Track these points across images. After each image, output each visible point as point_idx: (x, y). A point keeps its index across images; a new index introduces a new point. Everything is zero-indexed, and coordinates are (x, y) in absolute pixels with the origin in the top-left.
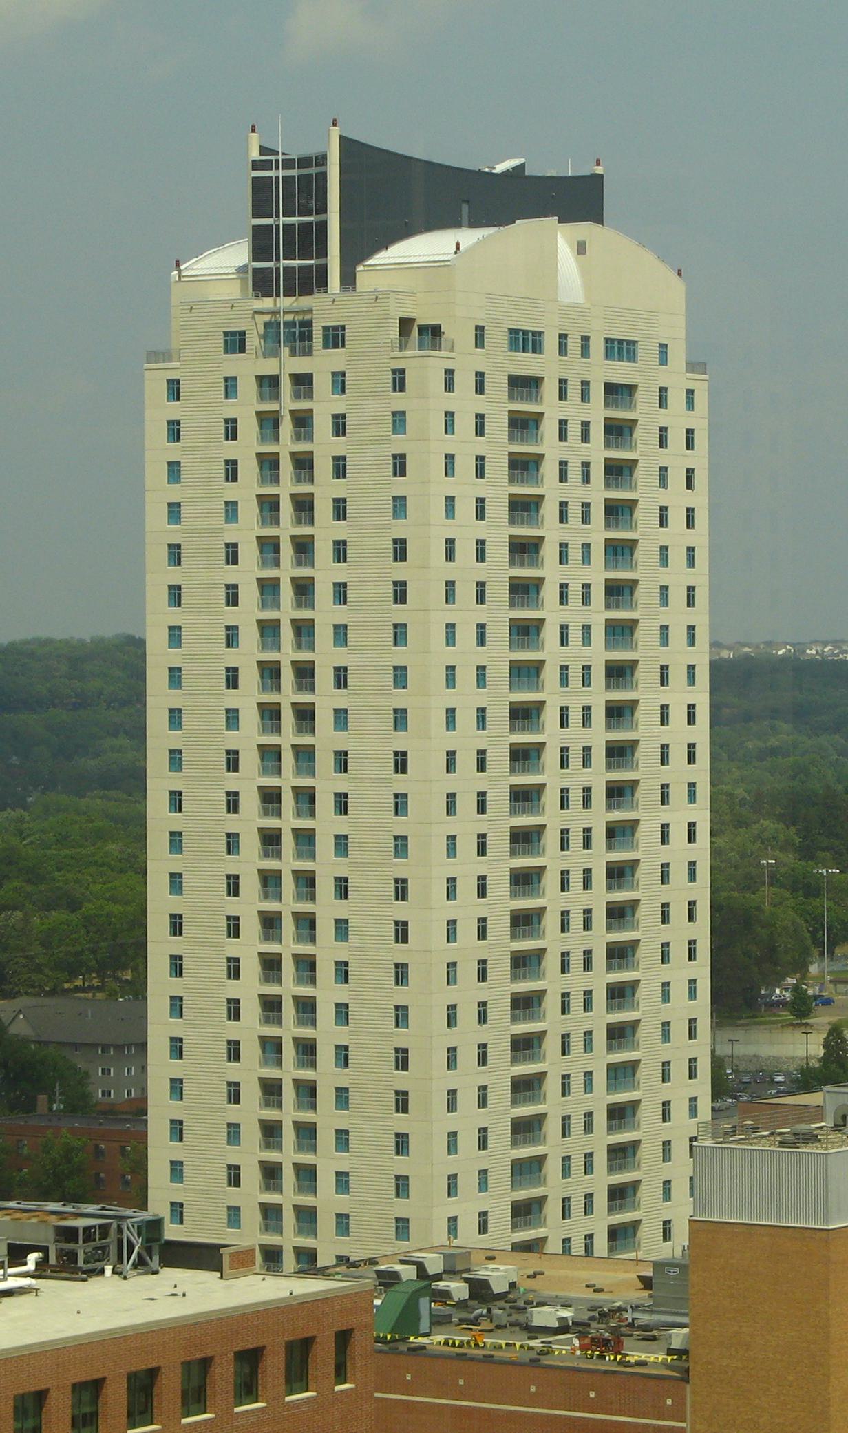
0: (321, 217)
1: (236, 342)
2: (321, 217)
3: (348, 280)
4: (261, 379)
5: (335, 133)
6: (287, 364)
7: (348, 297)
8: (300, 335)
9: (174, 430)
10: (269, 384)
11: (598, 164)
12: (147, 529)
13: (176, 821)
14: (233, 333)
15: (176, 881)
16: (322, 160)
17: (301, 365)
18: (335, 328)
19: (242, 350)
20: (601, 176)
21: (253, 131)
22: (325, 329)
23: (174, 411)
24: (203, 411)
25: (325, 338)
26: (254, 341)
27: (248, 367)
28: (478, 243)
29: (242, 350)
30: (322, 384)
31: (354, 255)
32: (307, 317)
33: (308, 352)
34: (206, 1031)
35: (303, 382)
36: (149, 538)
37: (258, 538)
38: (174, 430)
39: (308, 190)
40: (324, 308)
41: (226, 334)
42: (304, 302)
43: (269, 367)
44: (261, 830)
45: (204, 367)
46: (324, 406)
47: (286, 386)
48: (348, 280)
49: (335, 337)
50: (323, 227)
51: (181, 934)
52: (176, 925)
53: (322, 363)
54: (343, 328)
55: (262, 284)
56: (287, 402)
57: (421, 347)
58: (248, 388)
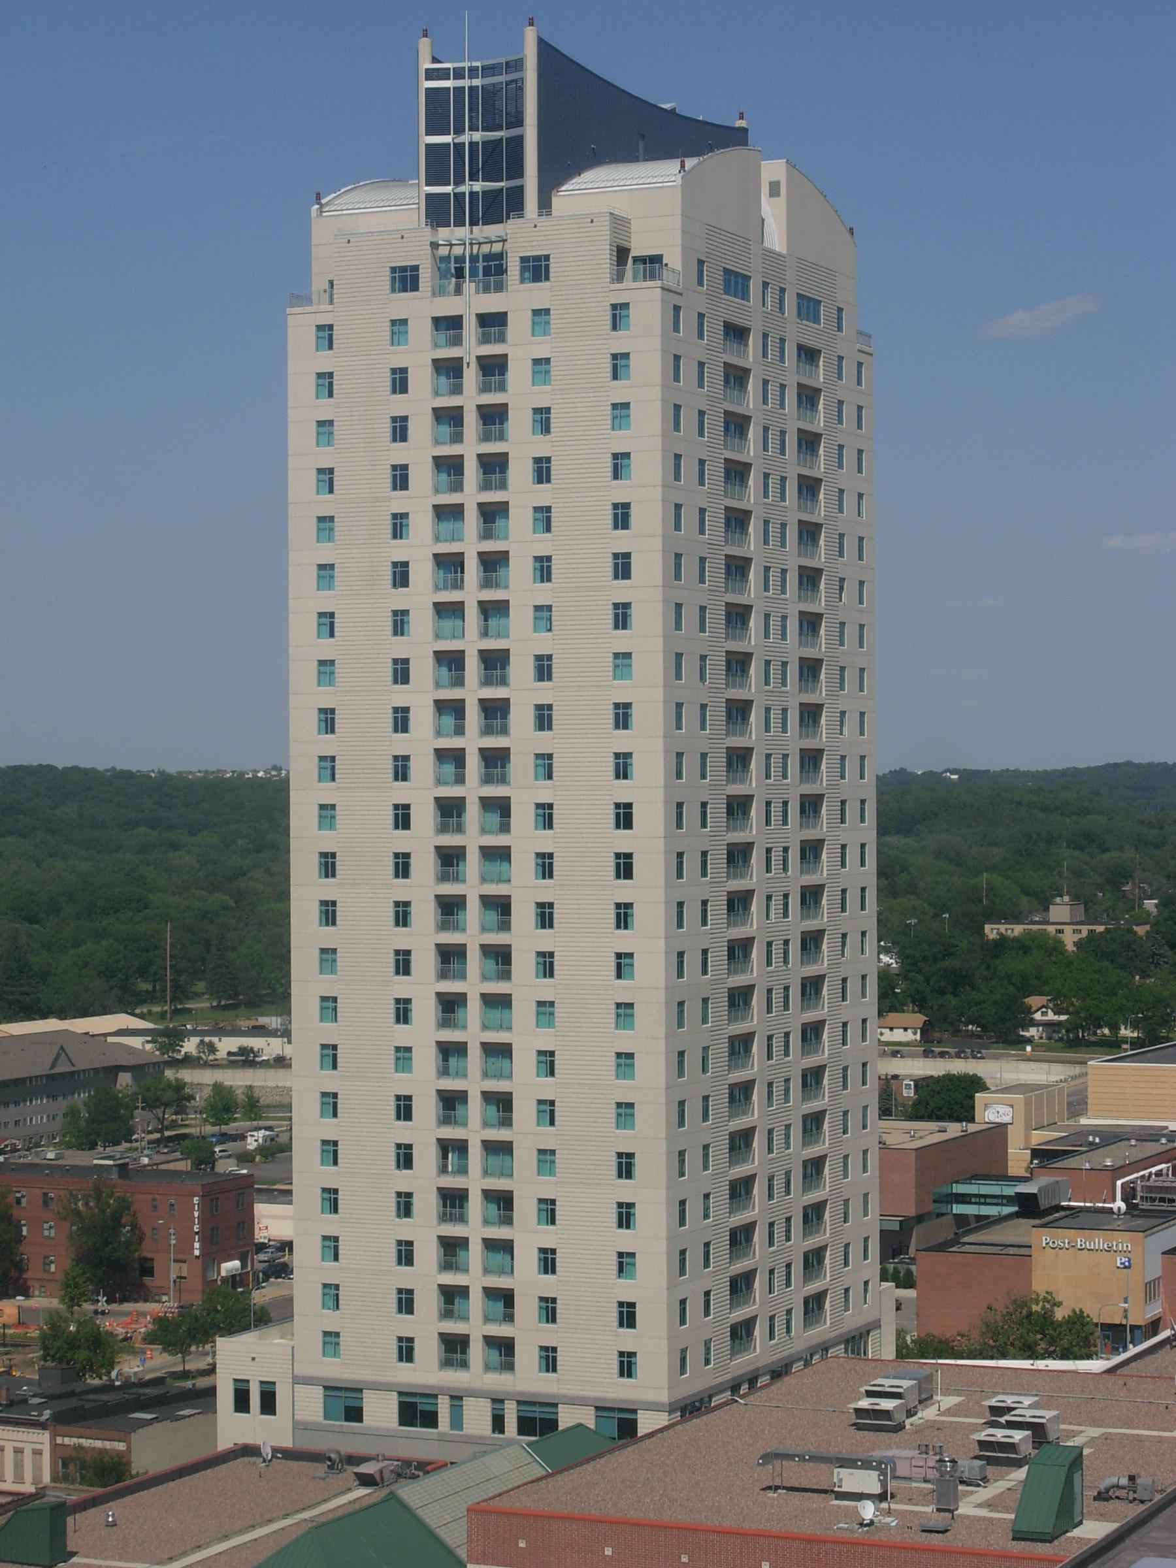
0: (514, 132)
1: (406, 279)
2: (514, 132)
3: (545, 204)
4: (438, 322)
5: (530, 37)
6: (472, 302)
7: (544, 222)
8: (492, 269)
9: (328, 622)
10: (449, 325)
11: (741, 118)
12: (290, 500)
13: (328, 936)
14: (403, 269)
15: (329, 913)
16: (517, 65)
17: (491, 303)
18: (537, 258)
19: (415, 288)
20: (745, 130)
21: (425, 35)
22: (524, 260)
23: (325, 361)
24: (363, 361)
25: (523, 269)
26: (426, 277)
27: (421, 308)
28: (698, 164)
29: (415, 288)
30: (519, 324)
31: (550, 182)
32: (497, 248)
33: (500, 287)
34: (366, 1030)
35: (493, 323)
36: (292, 510)
37: (434, 506)
38: (328, 622)
39: (498, 106)
40: (519, 236)
41: (393, 270)
42: (493, 231)
43: (449, 306)
44: (438, 848)
45: (365, 309)
46: (519, 347)
47: (470, 328)
48: (545, 204)
49: (537, 269)
50: (517, 144)
51: (334, 876)
52: (328, 865)
53: (517, 298)
54: (547, 258)
55: (438, 212)
56: (471, 348)
57: (635, 279)
58: (421, 331)
